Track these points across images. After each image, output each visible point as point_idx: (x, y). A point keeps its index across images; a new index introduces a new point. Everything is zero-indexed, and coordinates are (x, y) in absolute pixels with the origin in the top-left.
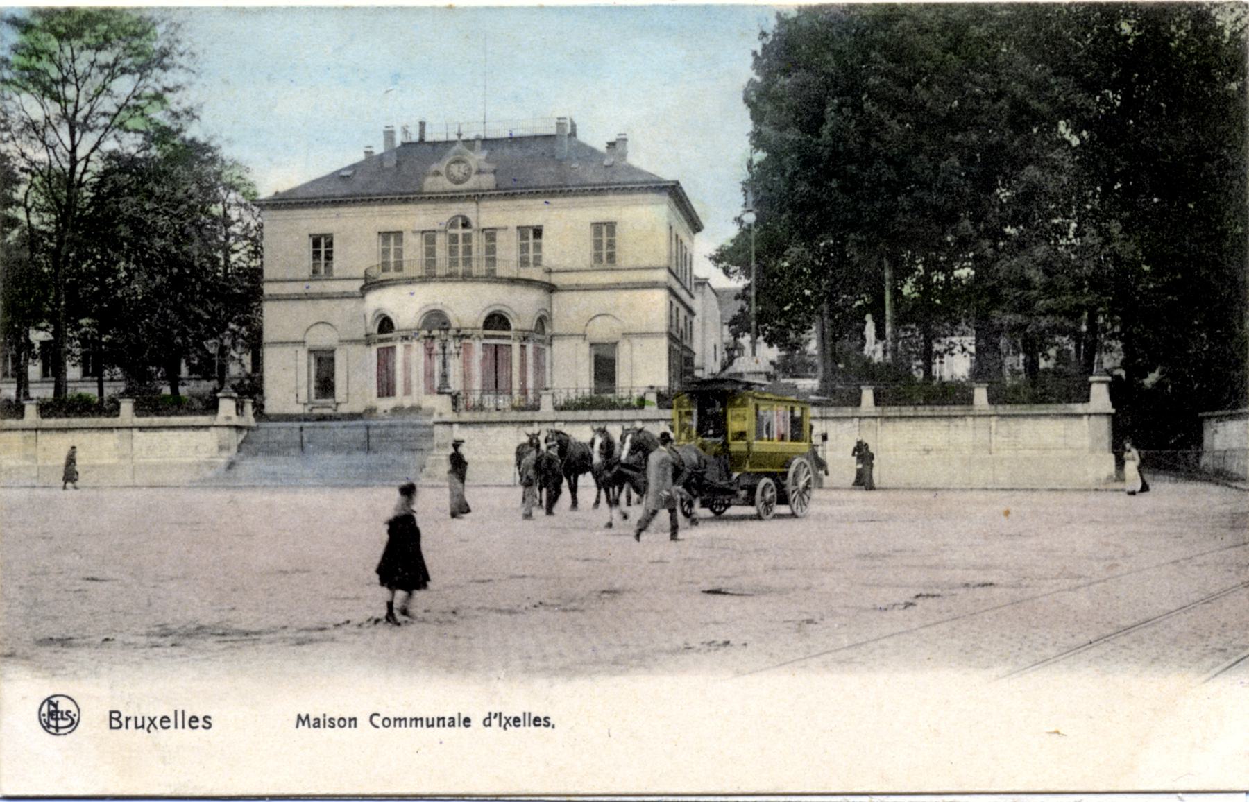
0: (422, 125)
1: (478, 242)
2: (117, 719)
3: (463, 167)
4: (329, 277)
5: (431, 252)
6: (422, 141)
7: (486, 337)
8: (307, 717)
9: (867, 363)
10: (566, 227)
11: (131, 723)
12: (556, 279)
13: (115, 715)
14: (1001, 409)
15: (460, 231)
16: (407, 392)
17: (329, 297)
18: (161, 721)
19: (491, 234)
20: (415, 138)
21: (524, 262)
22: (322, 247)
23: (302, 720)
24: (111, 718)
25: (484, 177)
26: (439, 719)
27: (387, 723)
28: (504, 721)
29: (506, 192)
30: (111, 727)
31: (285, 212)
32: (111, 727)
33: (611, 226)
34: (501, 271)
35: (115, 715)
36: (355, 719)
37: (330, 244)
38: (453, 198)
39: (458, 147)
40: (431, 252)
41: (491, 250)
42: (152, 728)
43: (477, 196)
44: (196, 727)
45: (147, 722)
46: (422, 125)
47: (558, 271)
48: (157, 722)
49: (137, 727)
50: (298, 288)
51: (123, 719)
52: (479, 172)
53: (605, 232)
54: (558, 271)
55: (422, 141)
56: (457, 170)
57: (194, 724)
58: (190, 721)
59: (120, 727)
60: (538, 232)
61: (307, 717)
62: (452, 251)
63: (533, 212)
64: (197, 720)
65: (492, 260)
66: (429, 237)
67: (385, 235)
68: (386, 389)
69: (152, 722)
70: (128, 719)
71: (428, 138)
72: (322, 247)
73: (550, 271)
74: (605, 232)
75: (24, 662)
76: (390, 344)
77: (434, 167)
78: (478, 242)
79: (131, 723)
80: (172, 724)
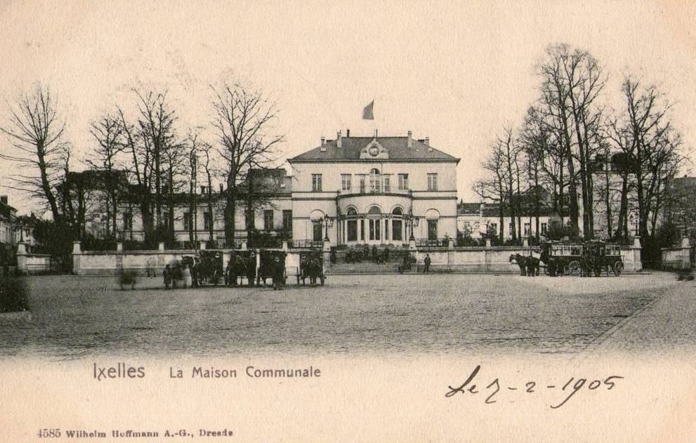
0: (348, 131)
3: (375, 149)
4: (320, 191)
7: (394, 217)
8: (200, 369)
10: (418, 175)
12: (414, 195)
14: (495, 247)
16: (363, 238)
18: (109, 371)
22: (317, 179)
23: (573, 379)
25: (384, 154)
26: (292, 375)
27: (258, 373)
28: (98, 373)
29: (392, 160)
31: (317, 165)
33: (406, 176)
34: (392, 191)
36: (235, 371)
39: (374, 141)
42: (102, 376)
43: (382, 161)
44: (134, 376)
46: (348, 131)
47: (415, 192)
48: (106, 372)
49: (288, 376)
50: (310, 195)
52: (382, 152)
54: (415, 192)
56: (374, 150)
57: (132, 374)
58: (129, 372)
59: (260, 376)
60: (406, 176)
61: (200, 369)
64: (135, 371)
68: (352, 237)
69: (102, 372)
71: (351, 136)
72: (317, 179)
73: (411, 191)
75: (271, 348)
76: (355, 219)
77: (364, 149)
80: (117, 374)
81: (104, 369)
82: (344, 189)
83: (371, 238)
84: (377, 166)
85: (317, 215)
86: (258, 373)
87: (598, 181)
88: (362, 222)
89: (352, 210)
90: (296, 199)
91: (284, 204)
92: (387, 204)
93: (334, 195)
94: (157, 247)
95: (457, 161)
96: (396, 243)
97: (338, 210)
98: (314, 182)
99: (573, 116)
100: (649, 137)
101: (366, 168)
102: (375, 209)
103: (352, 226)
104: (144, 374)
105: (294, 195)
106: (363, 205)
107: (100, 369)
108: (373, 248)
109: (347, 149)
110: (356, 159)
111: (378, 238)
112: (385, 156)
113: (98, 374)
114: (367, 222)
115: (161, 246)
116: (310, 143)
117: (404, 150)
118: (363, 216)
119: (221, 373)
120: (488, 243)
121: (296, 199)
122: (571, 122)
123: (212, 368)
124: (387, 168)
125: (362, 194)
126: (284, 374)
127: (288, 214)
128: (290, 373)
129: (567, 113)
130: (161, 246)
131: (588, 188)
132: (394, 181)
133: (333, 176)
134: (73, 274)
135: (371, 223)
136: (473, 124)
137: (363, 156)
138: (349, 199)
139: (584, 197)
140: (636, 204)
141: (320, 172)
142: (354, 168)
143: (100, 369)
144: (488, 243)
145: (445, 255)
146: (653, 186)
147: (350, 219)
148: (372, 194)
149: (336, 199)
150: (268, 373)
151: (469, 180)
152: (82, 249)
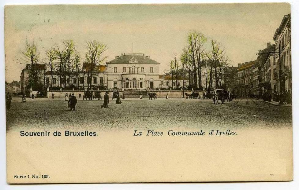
0: (124, 53)
1: (136, 69)
2: (68, 133)
5: (130, 70)
6: (124, 55)
9: (197, 88)
10: (147, 67)
11: (72, 134)
13: (67, 132)
15: (134, 68)
16: (131, 87)
17: (153, 75)
19: (138, 68)
20: (123, 55)
21: (142, 72)
24: (66, 133)
30: (66, 135)
32: (66, 135)
35: (67, 132)
37: (152, 69)
38: (134, 63)
40: (130, 70)
41: (138, 70)
45: (77, 134)
46: (124, 53)
48: (80, 134)
49: (30, 135)
50: (113, 74)
51: (70, 133)
53: (152, 69)
55: (124, 55)
60: (143, 68)
62: (133, 70)
63: (143, 66)
65: (137, 72)
66: (130, 68)
67: (124, 68)
70: (71, 133)
73: (145, 73)
74: (152, 69)
78: (136, 69)
79: (72, 134)
80: (84, 135)
81: (80, 133)
82: (124, 72)
83: (133, 87)
84: (134, 65)
85: (115, 80)
86: (171, 133)
87: (203, 70)
88: (130, 82)
89: (127, 79)
90: (109, 75)
91: (101, 75)
92: (138, 77)
93: (121, 74)
94: (72, 90)
95: (160, 64)
96: (141, 89)
97: (122, 79)
98: (151, 70)
99: (195, 51)
100: (219, 57)
101: (131, 66)
102: (134, 79)
103: (127, 83)
104: (21, 133)
105: (108, 74)
106: (131, 77)
107: (78, 133)
108: (128, 89)
109: (123, 59)
110: (127, 63)
111: (135, 87)
112: (137, 62)
113: (23, 134)
114: (132, 82)
115: (73, 89)
116: (112, 58)
117: (142, 60)
118: (131, 81)
119: (93, 134)
120: (171, 89)
121: (109, 75)
122: (195, 53)
123: (46, 131)
124: (137, 66)
125: (130, 74)
126: (30, 134)
127: (101, 79)
128: (43, 134)
129: (194, 50)
130: (73, 89)
131: (200, 72)
132: (140, 70)
133: (120, 67)
134: (47, 97)
135: (133, 82)
136: (166, 54)
137: (130, 62)
138: (126, 75)
139: (199, 74)
140: (215, 77)
141: (116, 67)
142: (127, 66)
143: (78, 133)
144: (171, 89)
145: (158, 92)
146: (220, 71)
147: (125, 82)
148: (133, 74)
149: (122, 75)
150: (179, 134)
151: (164, 68)
152: (50, 90)
